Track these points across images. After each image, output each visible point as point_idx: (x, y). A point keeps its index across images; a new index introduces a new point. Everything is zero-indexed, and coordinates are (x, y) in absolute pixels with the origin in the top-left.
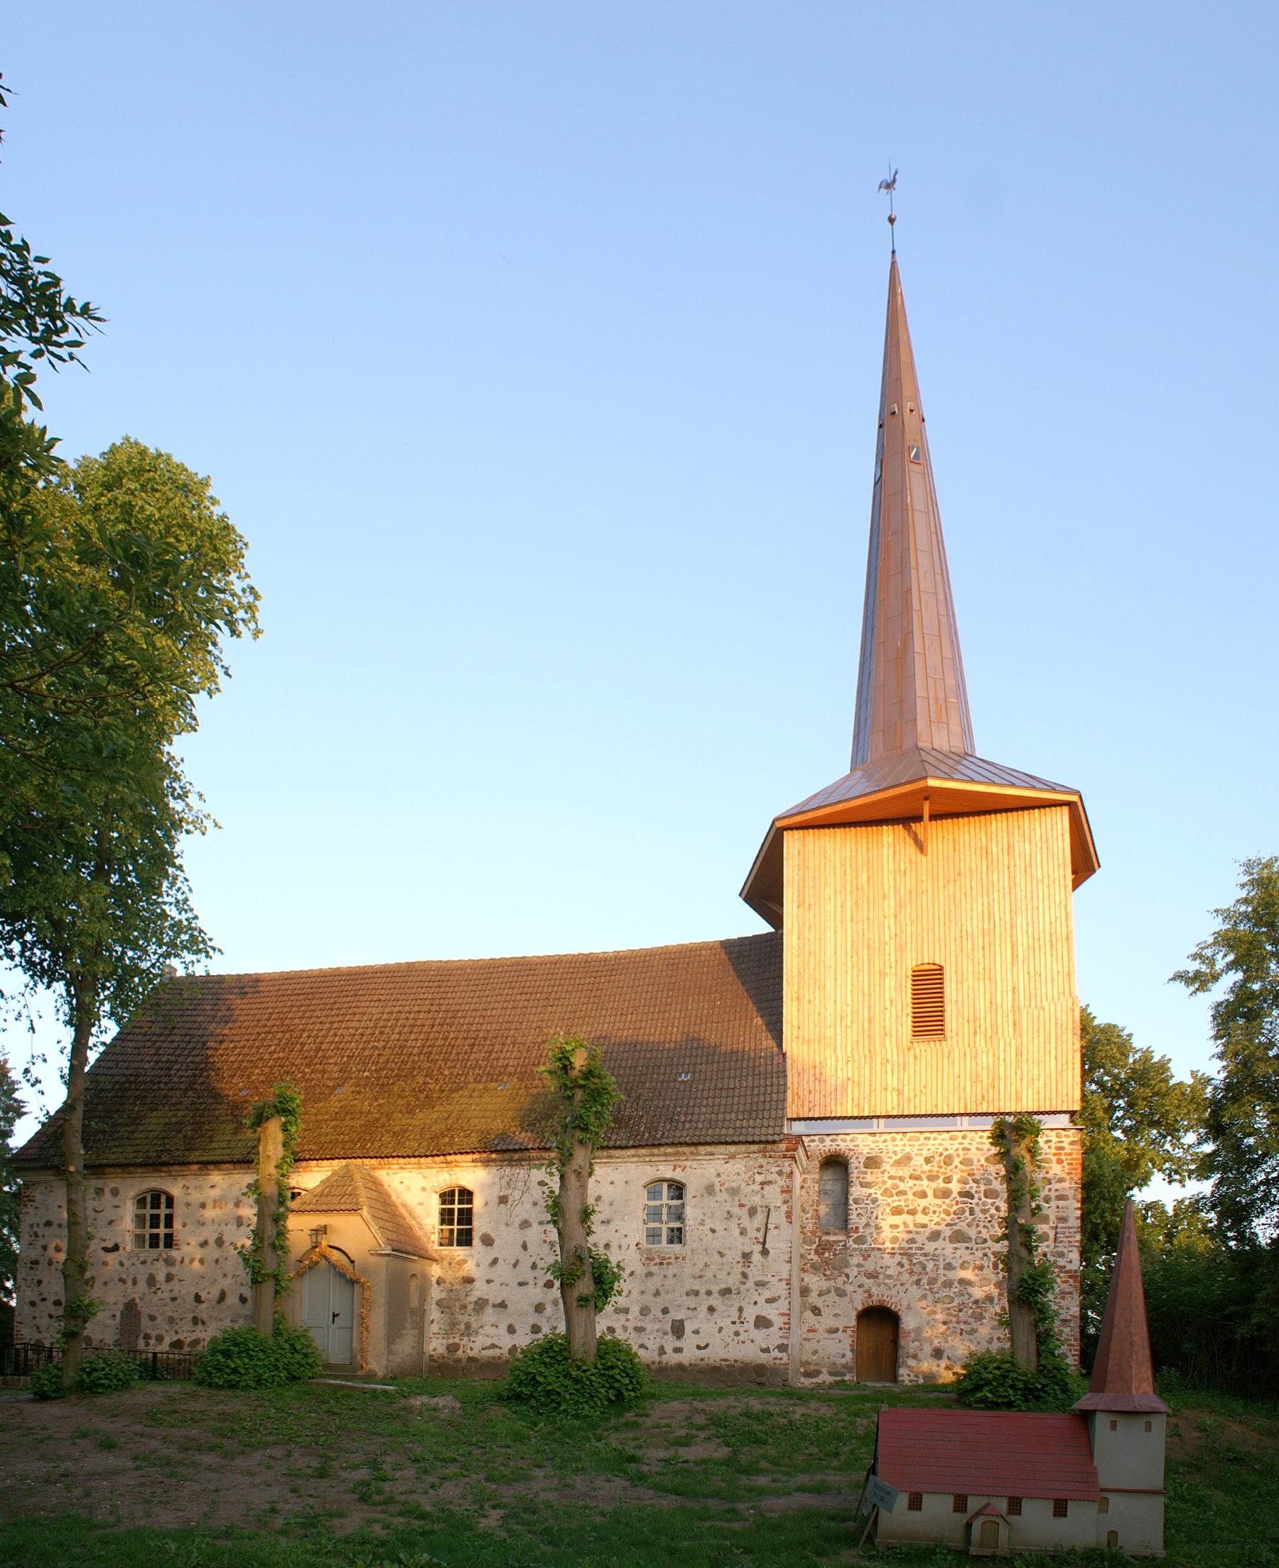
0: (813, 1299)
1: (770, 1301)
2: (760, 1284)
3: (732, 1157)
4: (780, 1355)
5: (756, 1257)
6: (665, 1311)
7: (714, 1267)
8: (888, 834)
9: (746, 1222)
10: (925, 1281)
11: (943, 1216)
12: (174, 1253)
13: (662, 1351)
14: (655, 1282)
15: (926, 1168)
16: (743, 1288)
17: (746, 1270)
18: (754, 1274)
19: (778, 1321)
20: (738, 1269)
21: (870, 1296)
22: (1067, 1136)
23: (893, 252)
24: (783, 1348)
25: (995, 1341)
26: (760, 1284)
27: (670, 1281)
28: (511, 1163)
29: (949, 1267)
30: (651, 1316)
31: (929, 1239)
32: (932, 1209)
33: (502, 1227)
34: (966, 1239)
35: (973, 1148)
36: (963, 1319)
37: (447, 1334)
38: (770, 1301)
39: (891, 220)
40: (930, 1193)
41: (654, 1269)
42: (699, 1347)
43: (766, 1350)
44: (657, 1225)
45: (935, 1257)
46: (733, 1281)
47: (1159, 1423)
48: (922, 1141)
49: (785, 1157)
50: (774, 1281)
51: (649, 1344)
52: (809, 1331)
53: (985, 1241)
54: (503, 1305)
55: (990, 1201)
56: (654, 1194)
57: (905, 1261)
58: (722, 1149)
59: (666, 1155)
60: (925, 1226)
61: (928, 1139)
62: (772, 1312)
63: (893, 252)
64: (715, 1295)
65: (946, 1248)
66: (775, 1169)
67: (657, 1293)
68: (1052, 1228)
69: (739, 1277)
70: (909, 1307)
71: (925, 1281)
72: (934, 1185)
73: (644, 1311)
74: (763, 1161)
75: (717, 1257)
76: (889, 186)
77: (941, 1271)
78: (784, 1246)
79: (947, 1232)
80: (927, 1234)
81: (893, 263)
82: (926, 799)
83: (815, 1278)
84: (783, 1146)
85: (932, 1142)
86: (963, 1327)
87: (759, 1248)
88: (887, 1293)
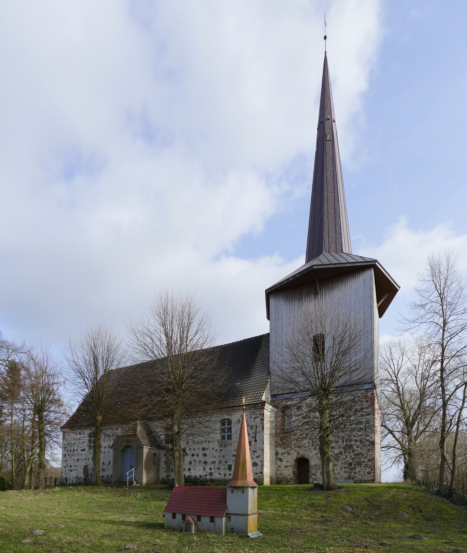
0: (280, 456)
4: (261, 475)
6: (226, 462)
14: (223, 452)
21: (299, 454)
23: (326, 52)
25: (343, 468)
27: (228, 452)
30: (222, 464)
37: (167, 472)
41: (222, 448)
44: (224, 434)
47: (256, 489)
51: (221, 473)
52: (279, 467)
56: (223, 424)
57: (310, 441)
63: (326, 52)
66: (258, 413)
67: (224, 456)
68: (364, 426)
70: (312, 457)
73: (220, 462)
74: (255, 410)
81: (326, 57)
87: (254, 439)
88: (304, 453)
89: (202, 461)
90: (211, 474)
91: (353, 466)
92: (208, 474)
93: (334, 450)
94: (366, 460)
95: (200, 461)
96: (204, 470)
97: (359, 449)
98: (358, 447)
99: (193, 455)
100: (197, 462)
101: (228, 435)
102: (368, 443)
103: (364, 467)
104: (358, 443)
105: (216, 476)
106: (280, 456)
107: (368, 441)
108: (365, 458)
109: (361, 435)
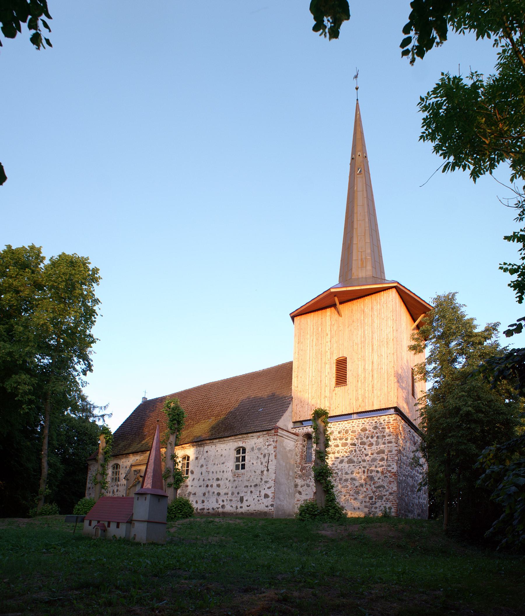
0: (299, 488)
1: (269, 488)
2: (266, 482)
3: (259, 437)
5: (265, 472)
6: (238, 493)
7: (252, 477)
8: (329, 312)
9: (263, 460)
10: (338, 479)
11: (345, 453)
12: (119, 483)
13: (237, 508)
14: (236, 482)
15: (339, 435)
16: (261, 484)
17: (262, 477)
18: (264, 479)
19: (271, 495)
20: (259, 478)
22: (392, 417)
23: (357, 100)
24: (272, 505)
25: (364, 502)
26: (266, 482)
27: (240, 482)
28: (200, 446)
29: (347, 473)
31: (339, 463)
32: (341, 451)
33: (196, 467)
34: (354, 462)
35: (356, 426)
36: (351, 494)
38: (269, 488)
39: (357, 89)
40: (340, 445)
41: (236, 479)
42: (247, 506)
43: (267, 506)
45: (342, 470)
46: (258, 481)
48: (337, 425)
49: (275, 435)
50: (270, 480)
53: (360, 462)
54: (195, 494)
55: (362, 446)
56: (238, 452)
58: (255, 434)
59: (239, 438)
60: (338, 458)
61: (339, 424)
62: (269, 492)
63: (357, 100)
64: (253, 487)
65: (345, 465)
67: (236, 487)
69: (260, 480)
71: (338, 479)
72: (341, 442)
73: (233, 494)
74: (268, 437)
75: (254, 473)
76: (356, 77)
77: (344, 475)
78: (274, 467)
79: (346, 460)
80: (339, 461)
81: (357, 104)
82: (335, 296)
83: (300, 481)
84: (273, 431)
85: (341, 425)
86: (352, 497)
87: (266, 469)
89: (216, 493)
90: (223, 506)
91: (374, 500)
92: (220, 506)
93: (354, 482)
94: (388, 493)
95: (214, 493)
96: (217, 502)
97: (380, 480)
98: (379, 479)
99: (207, 486)
100: (211, 493)
101: (242, 464)
102: (389, 474)
103: (385, 501)
104: (379, 475)
105: (228, 509)
106: (299, 488)
107: (390, 471)
108: (387, 491)
109: (383, 466)
